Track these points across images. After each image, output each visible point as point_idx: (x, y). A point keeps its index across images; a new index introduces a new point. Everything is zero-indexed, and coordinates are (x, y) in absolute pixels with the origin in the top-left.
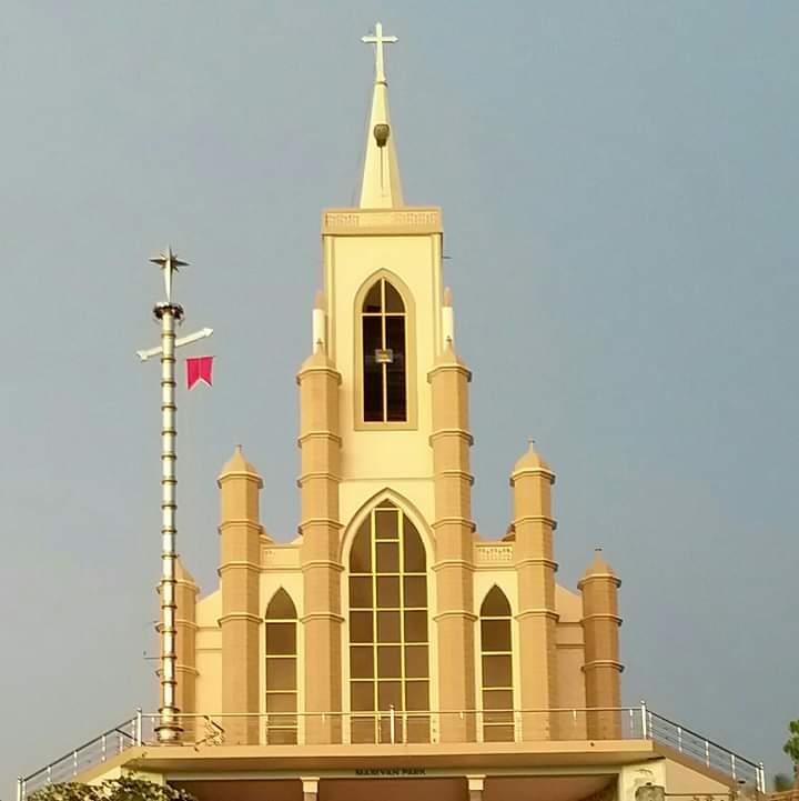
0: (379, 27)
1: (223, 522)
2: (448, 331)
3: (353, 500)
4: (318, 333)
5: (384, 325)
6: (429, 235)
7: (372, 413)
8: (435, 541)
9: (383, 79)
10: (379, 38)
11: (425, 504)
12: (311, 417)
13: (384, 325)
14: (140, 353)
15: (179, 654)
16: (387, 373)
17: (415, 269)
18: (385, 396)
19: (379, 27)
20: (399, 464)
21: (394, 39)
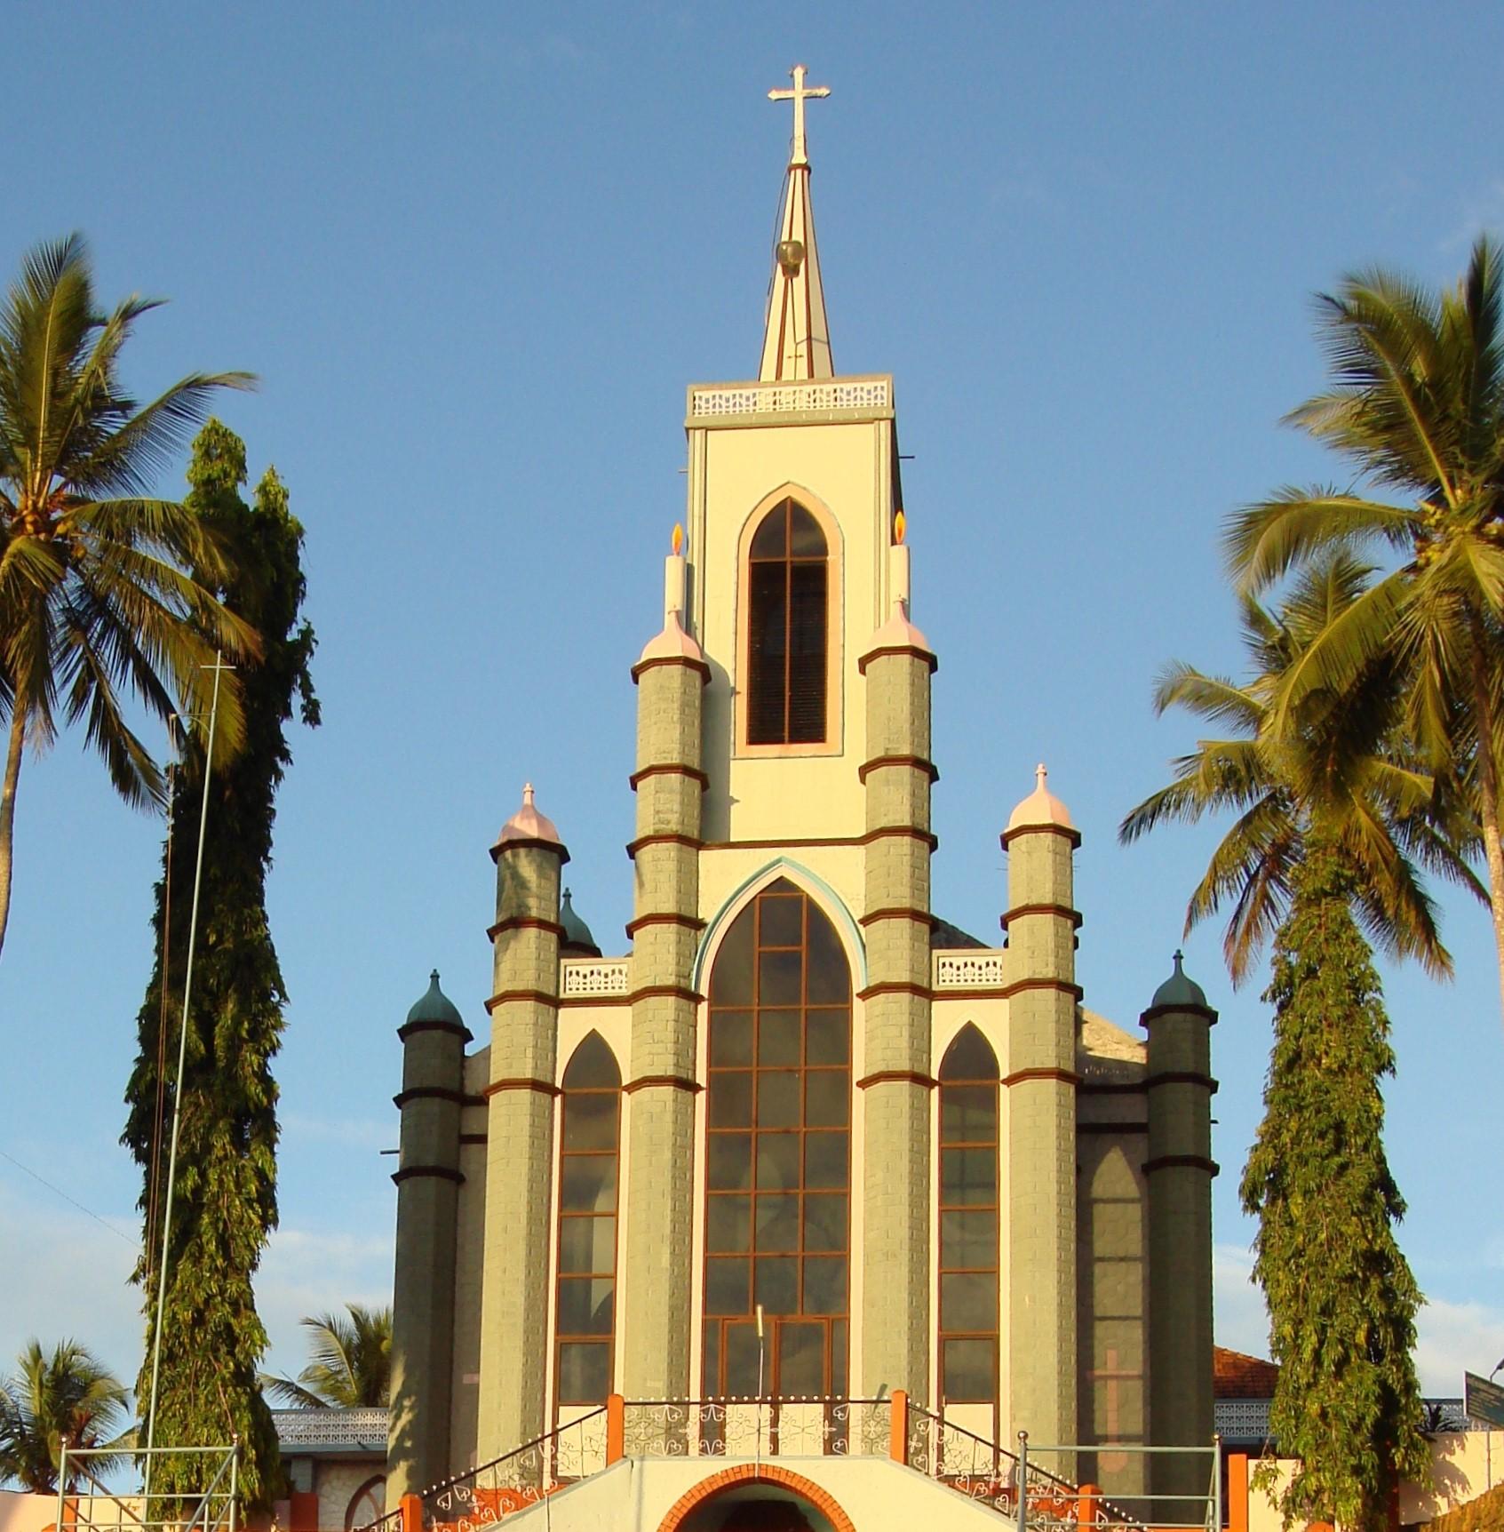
0: (799, 73)
1: (643, 659)
2: (898, 589)
3: (724, 883)
4: (673, 597)
5: (789, 576)
6: (871, 421)
7: (764, 731)
8: (864, 946)
9: (803, 160)
10: (798, 93)
11: (841, 887)
12: (660, 731)
13: (789, 576)
14: (289, 638)
15: (819, 331)
16: (941, 1150)
17: (841, 482)
18: (788, 697)
19: (799, 73)
20: (802, 810)
21: (824, 91)
